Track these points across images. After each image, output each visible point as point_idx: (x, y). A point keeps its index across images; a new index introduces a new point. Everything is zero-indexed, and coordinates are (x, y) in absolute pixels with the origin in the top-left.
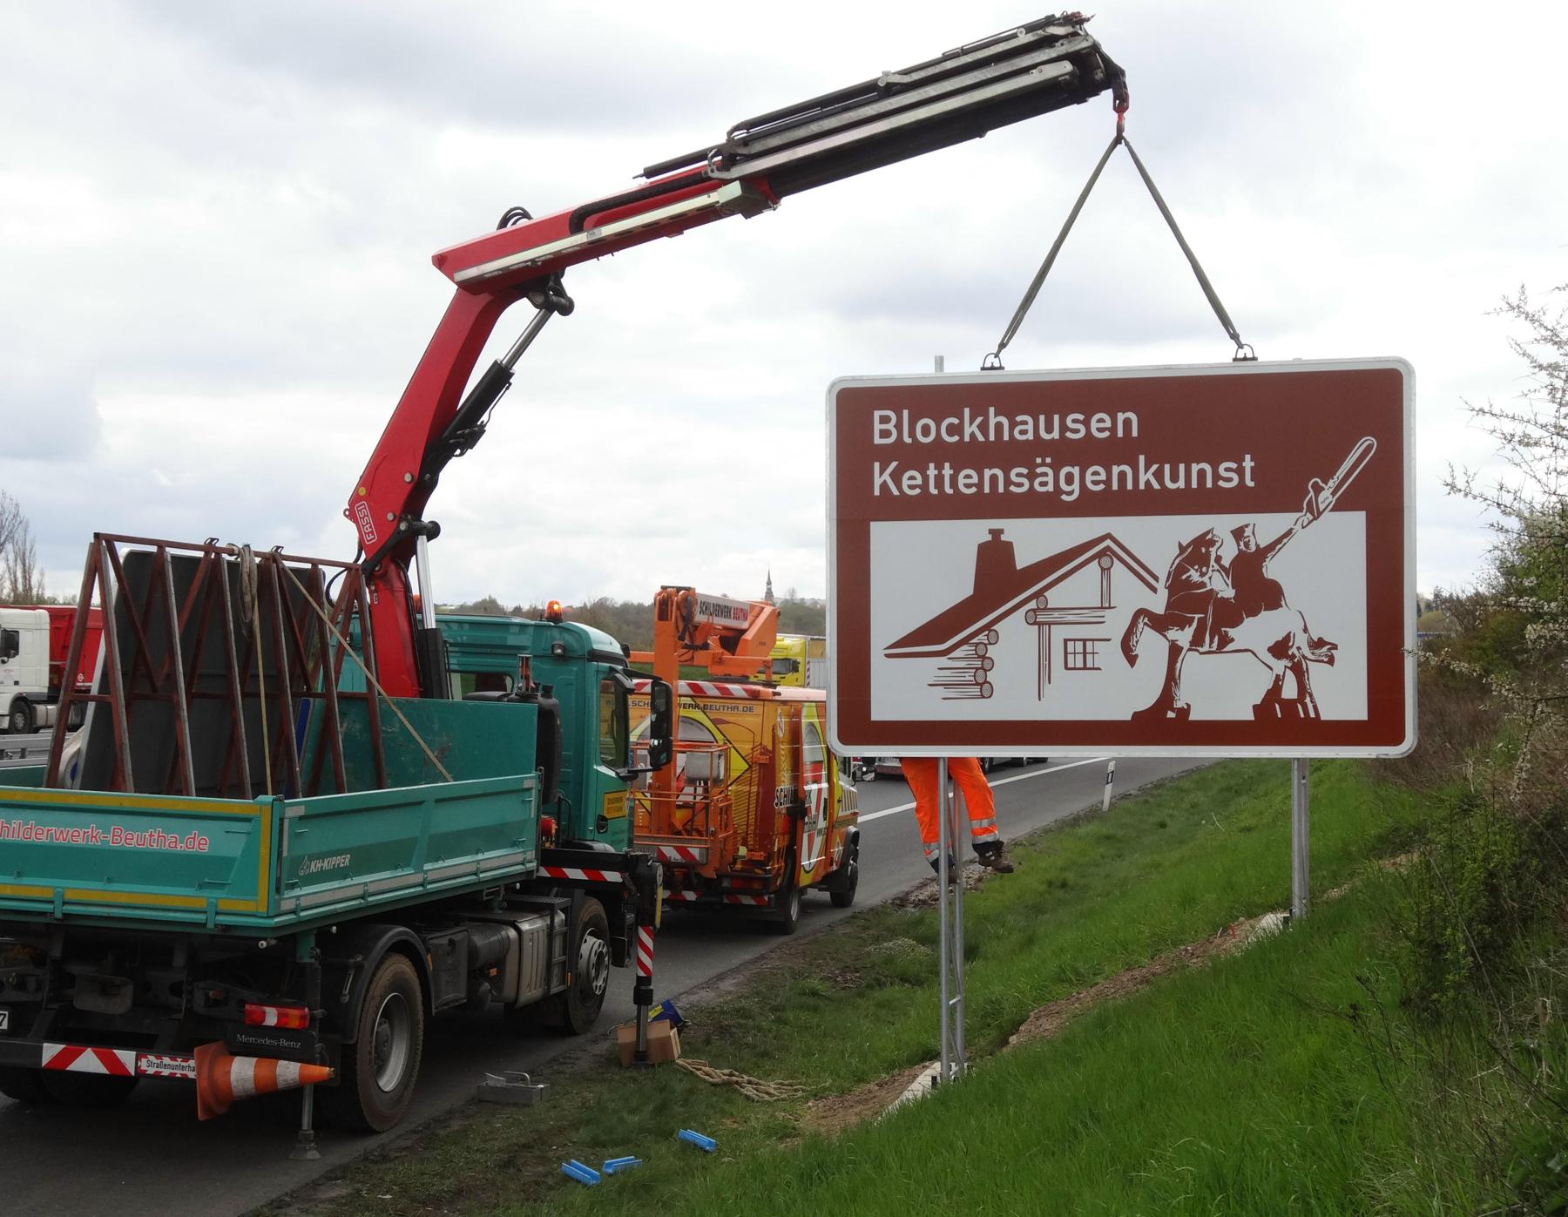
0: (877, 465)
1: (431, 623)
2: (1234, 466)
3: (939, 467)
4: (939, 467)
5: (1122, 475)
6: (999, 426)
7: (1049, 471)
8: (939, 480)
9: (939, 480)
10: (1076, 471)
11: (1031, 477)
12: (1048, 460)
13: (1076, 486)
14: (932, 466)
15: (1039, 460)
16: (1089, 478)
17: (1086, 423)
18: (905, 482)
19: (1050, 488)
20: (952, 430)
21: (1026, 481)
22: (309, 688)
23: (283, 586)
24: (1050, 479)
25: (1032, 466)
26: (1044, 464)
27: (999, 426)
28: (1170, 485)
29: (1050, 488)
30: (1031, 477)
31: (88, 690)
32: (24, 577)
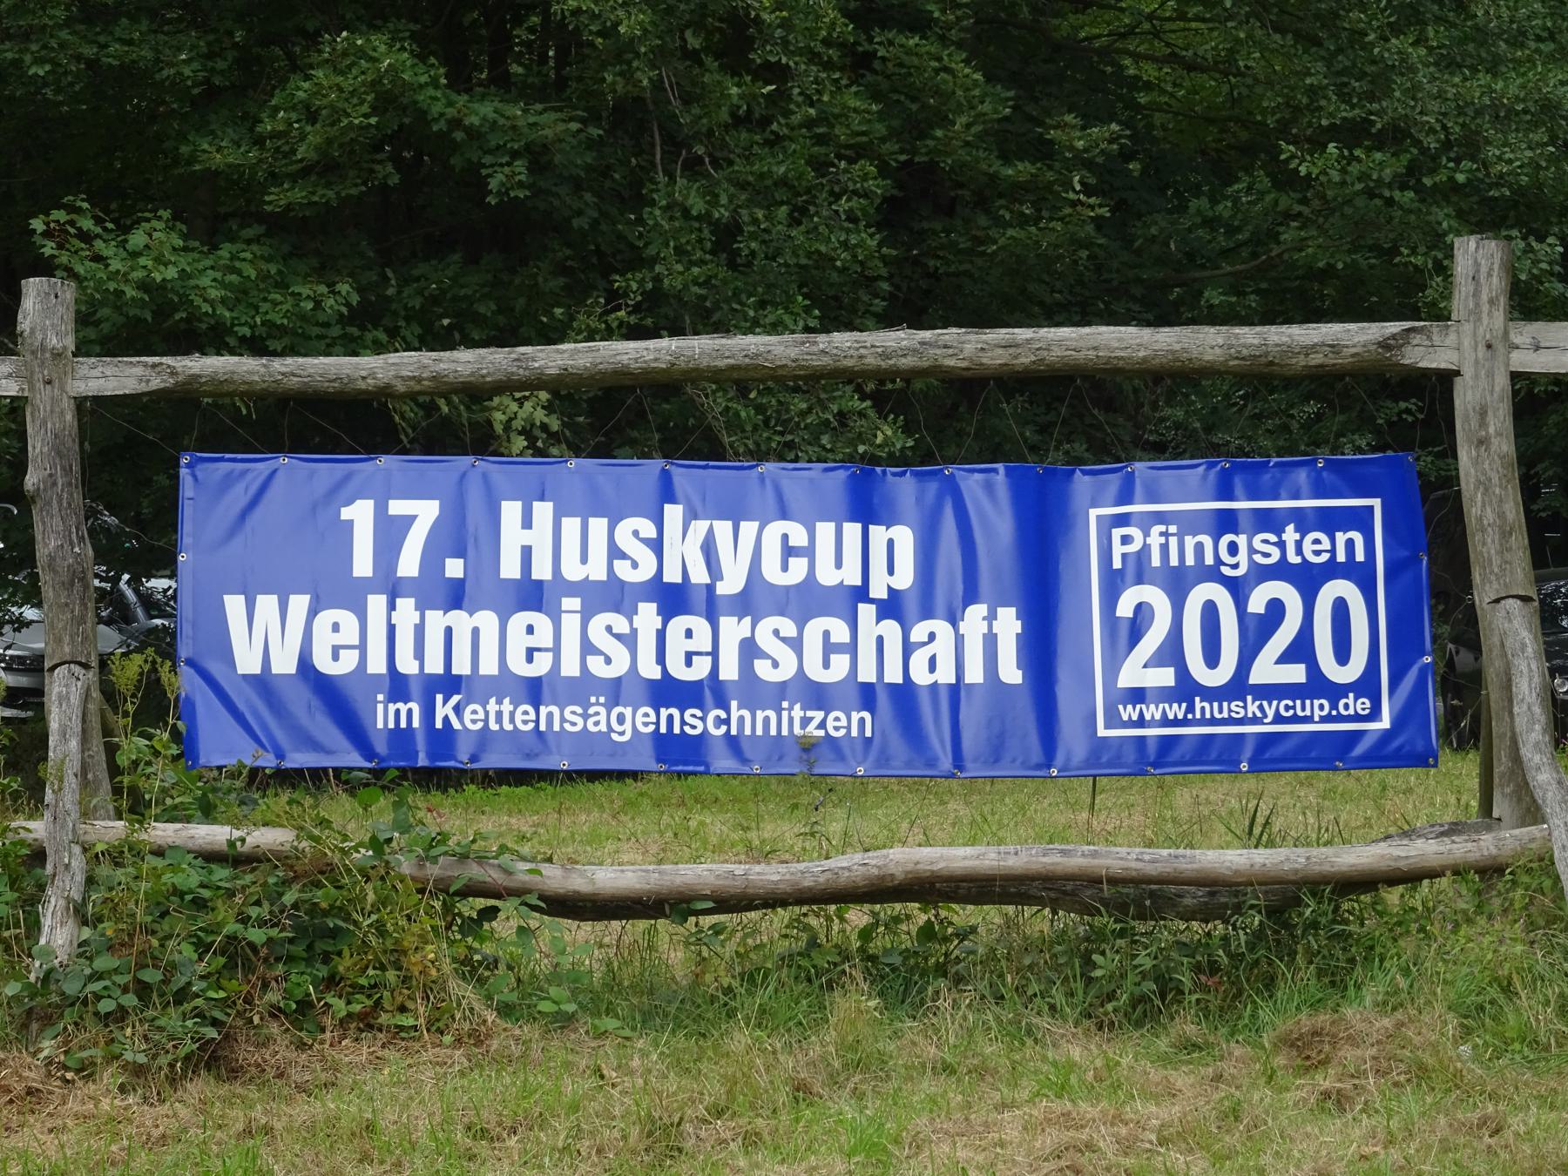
0: (439, 698)
1: (1448, 239)
2: (1273, 538)
3: (499, 702)
4: (499, 702)
5: (767, 720)
6: (741, 719)
7: (603, 710)
8: (499, 714)
9: (499, 714)
10: (628, 712)
11: (585, 716)
12: (602, 700)
13: (628, 726)
14: (493, 700)
15: (593, 699)
16: (639, 719)
17: (703, 719)
18: (467, 716)
19: (603, 727)
20: (719, 722)
21: (580, 721)
22: (1126, 155)
23: (871, 684)
24: (603, 718)
25: (586, 705)
26: (598, 703)
27: (741, 719)
28: (675, 712)
29: (603, 727)
30: (585, 716)
31: (881, 617)
32: (1464, 627)
